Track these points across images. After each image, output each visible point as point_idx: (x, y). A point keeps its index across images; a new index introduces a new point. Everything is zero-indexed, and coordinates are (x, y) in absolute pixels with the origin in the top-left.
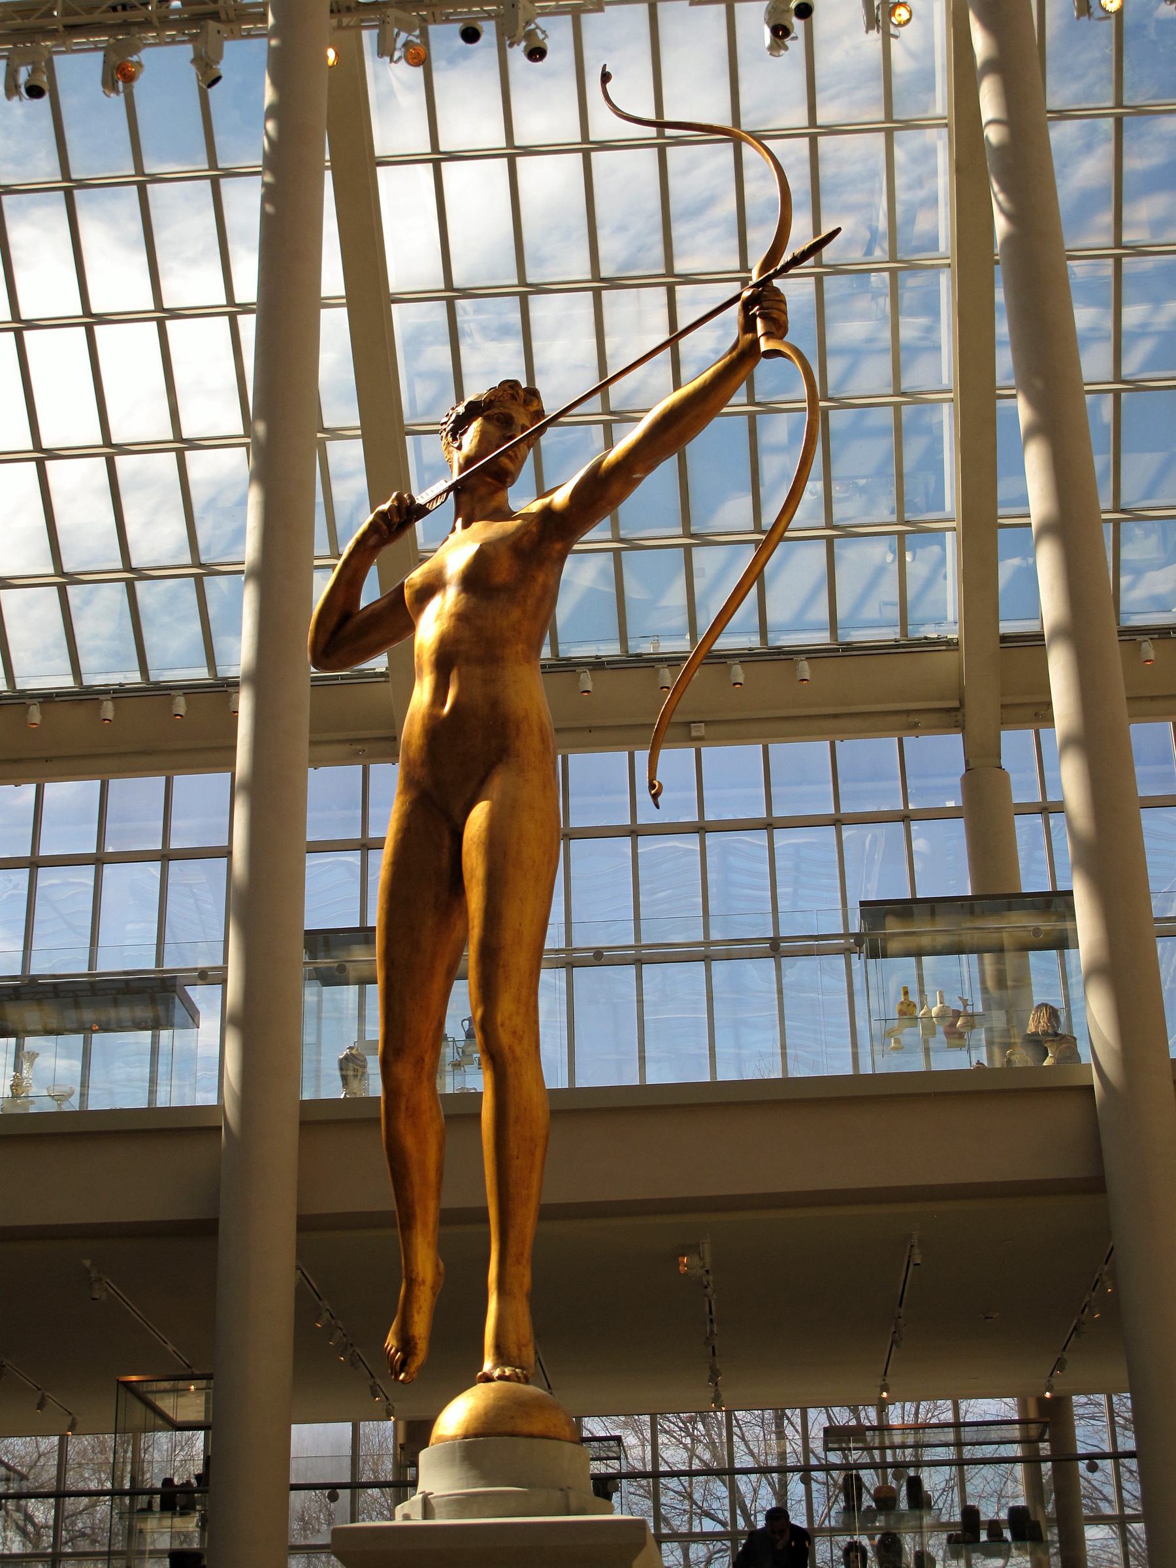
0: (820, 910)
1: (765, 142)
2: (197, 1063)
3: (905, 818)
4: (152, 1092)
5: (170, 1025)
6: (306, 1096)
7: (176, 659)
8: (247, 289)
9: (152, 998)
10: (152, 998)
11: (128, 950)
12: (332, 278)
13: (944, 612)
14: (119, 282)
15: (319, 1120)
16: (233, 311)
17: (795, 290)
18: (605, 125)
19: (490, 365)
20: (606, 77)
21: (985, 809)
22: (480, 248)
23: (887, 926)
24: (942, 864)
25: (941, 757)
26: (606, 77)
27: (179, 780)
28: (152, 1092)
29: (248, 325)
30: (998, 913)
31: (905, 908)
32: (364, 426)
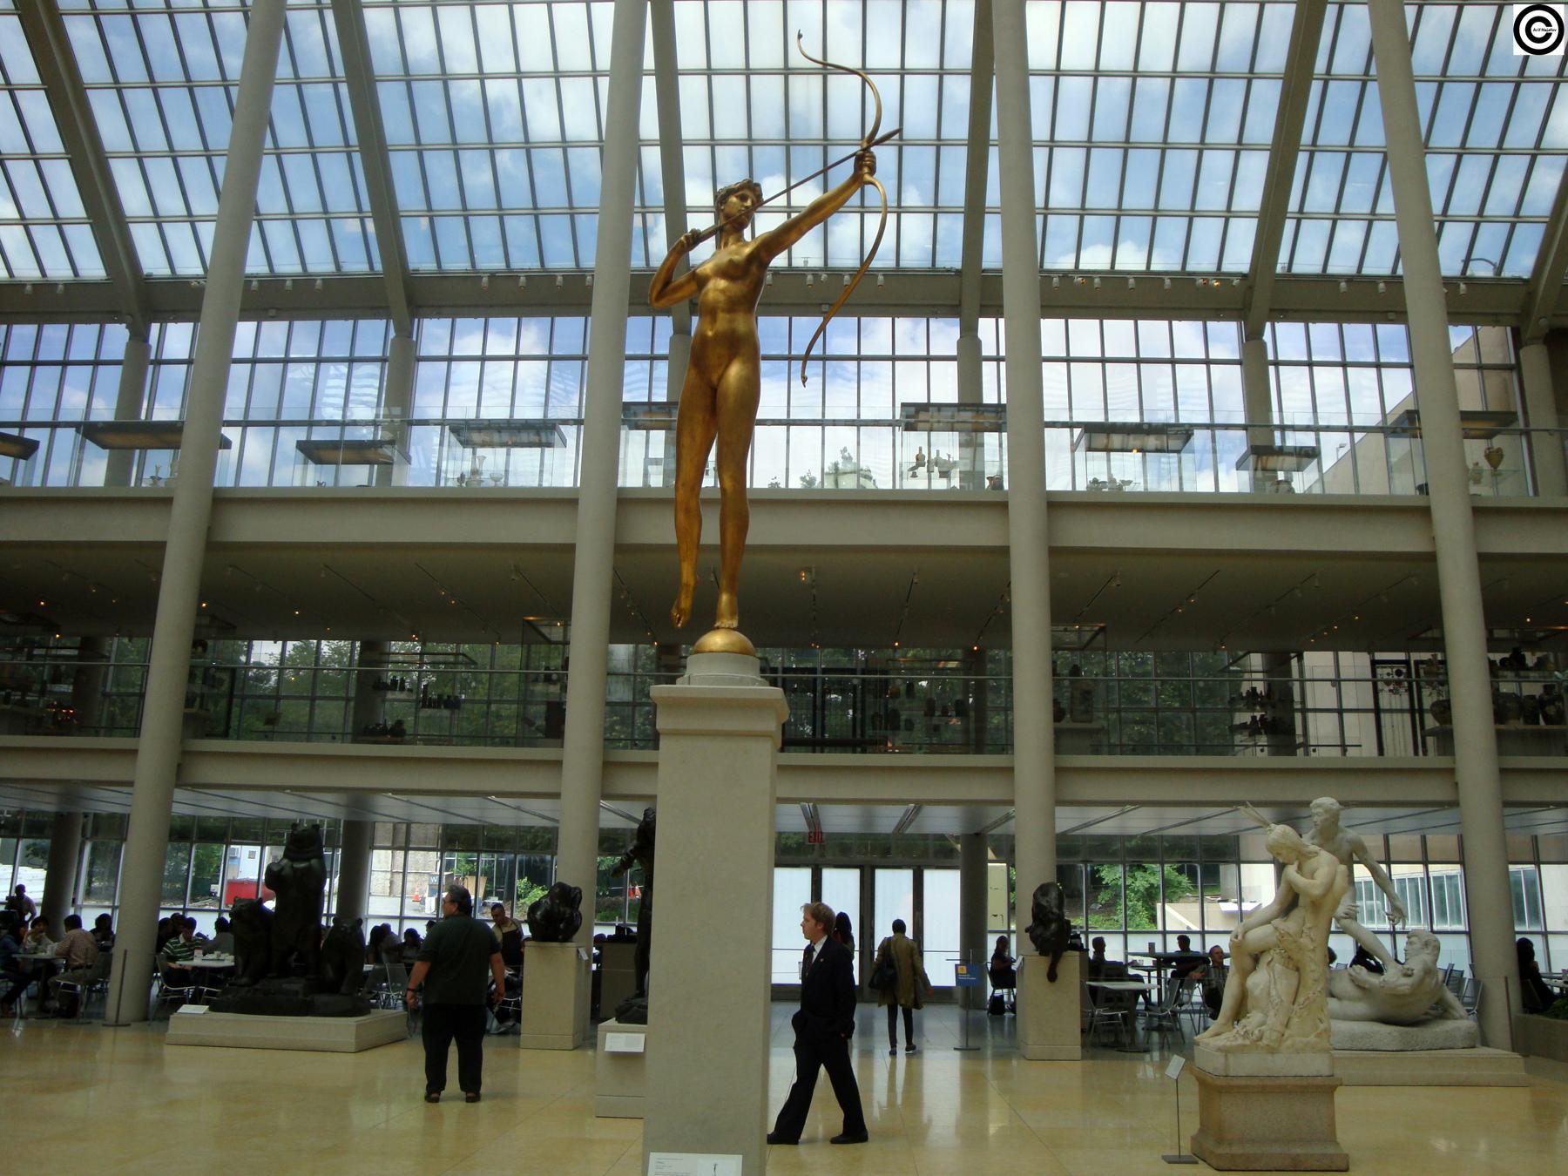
0: (879, 404)
1: (877, 137)
2: (559, 468)
3: (928, 359)
4: (541, 480)
5: (550, 445)
6: (620, 484)
7: (560, 259)
8: (604, 62)
9: (540, 433)
10: (540, 433)
11: (529, 411)
12: (649, 61)
13: (951, 257)
14: (539, 96)
15: (627, 502)
16: (595, 74)
17: (884, 156)
18: (796, 60)
19: (732, 175)
20: (800, 36)
21: (969, 358)
22: (731, 125)
23: (916, 417)
24: (945, 387)
25: (946, 335)
26: (800, 36)
27: (557, 319)
28: (541, 480)
29: (604, 83)
30: (971, 416)
31: (926, 407)
32: (666, 206)
